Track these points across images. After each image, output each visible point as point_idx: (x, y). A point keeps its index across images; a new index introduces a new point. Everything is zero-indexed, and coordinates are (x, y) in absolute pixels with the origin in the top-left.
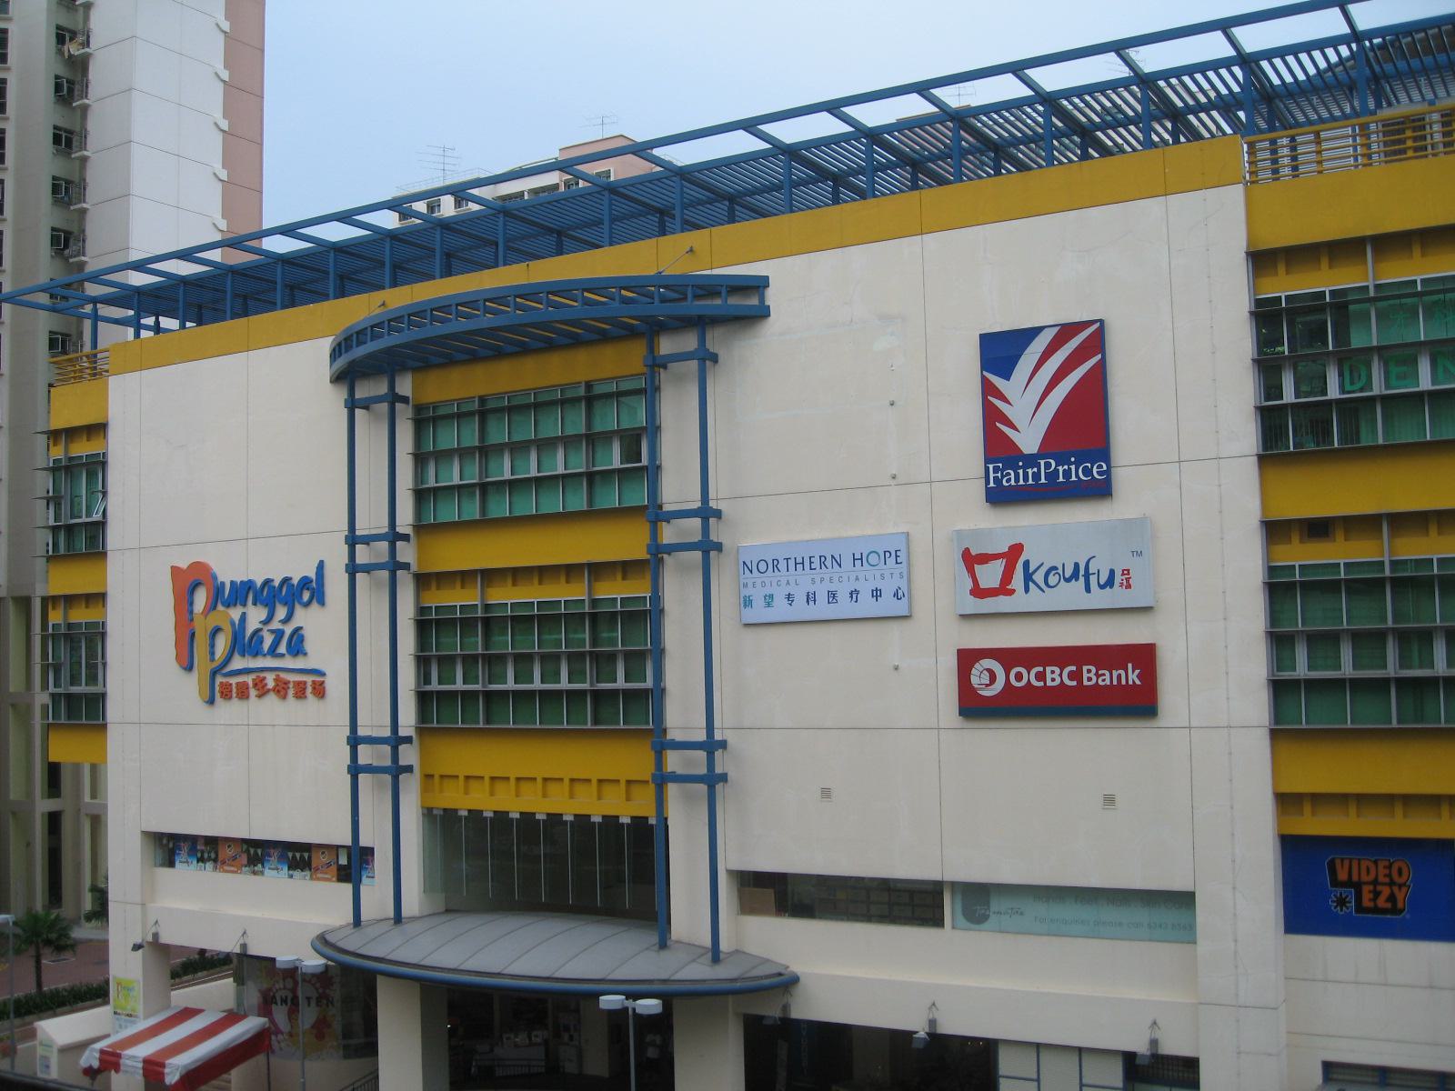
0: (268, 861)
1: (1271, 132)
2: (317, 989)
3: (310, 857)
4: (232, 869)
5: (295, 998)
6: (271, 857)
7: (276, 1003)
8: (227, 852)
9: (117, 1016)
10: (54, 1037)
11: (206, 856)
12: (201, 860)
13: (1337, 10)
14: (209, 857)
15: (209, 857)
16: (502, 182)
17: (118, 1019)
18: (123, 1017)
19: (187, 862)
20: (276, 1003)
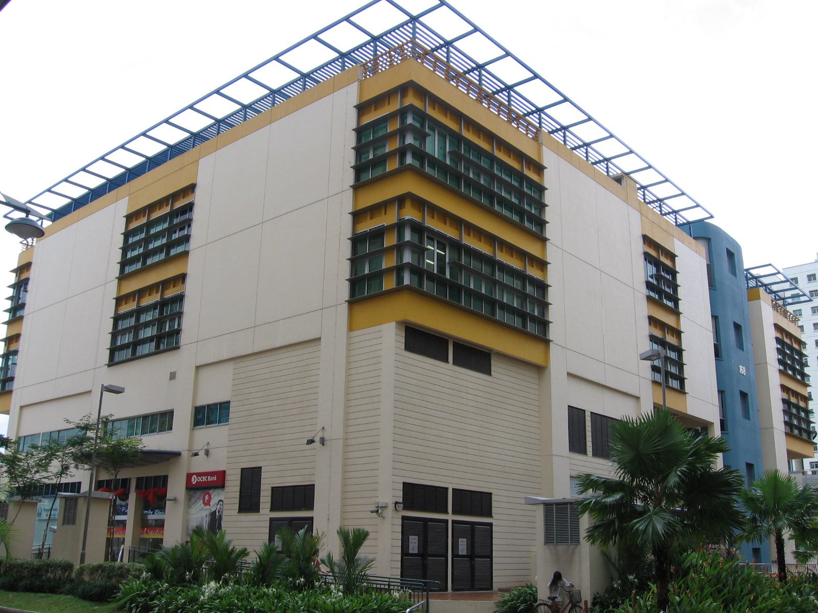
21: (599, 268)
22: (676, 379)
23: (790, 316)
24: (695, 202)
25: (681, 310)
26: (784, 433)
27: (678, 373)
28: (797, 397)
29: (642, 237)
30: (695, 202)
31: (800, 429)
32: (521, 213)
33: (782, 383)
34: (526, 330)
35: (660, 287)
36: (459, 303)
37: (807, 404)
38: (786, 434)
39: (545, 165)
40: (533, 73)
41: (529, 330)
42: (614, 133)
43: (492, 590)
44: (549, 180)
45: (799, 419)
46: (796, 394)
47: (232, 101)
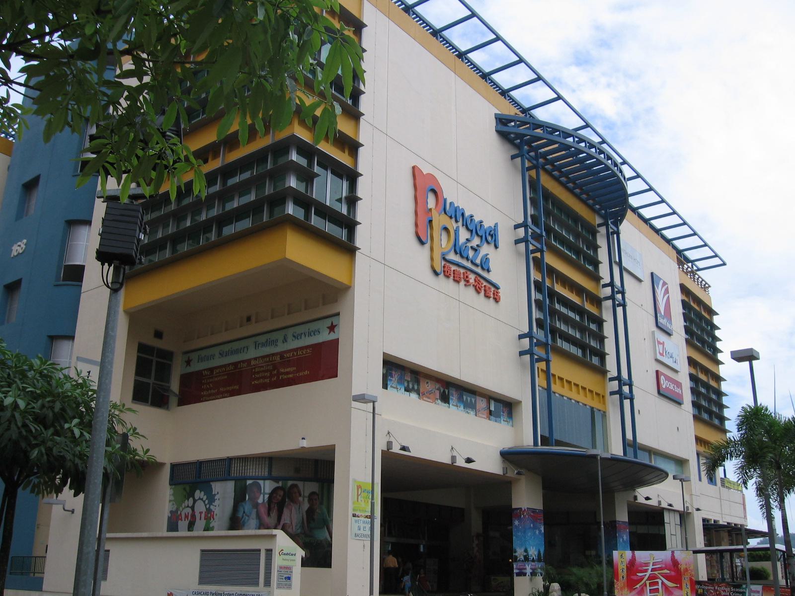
0: (391, 380)
1: (705, 529)
2: (206, 505)
3: (475, 401)
4: (429, 400)
5: (193, 516)
6: (392, 377)
7: (181, 520)
8: (427, 386)
9: (356, 518)
10: (707, 480)
11: (411, 386)
12: (407, 390)
13: (629, 198)
14: (413, 388)
15: (413, 388)
16: (446, 29)
17: (356, 521)
18: (363, 519)
19: (457, 406)
20: (181, 520)
21: (456, 180)
22: (596, 355)
23: (698, 279)
24: (693, 230)
25: (362, 109)
26: (692, 415)
27: (598, 348)
28: (706, 374)
29: (679, 285)
30: (693, 230)
31: (710, 413)
32: (578, 252)
33: (689, 356)
34: (586, 359)
35: (691, 328)
36: (308, 221)
37: (719, 385)
38: (694, 416)
39: (365, 22)
40: (683, 220)
41: (312, 223)
42: (544, 75)
43: (203, 551)
44: (368, 39)
45: (710, 400)
46: (706, 371)
47: (753, 394)
